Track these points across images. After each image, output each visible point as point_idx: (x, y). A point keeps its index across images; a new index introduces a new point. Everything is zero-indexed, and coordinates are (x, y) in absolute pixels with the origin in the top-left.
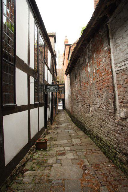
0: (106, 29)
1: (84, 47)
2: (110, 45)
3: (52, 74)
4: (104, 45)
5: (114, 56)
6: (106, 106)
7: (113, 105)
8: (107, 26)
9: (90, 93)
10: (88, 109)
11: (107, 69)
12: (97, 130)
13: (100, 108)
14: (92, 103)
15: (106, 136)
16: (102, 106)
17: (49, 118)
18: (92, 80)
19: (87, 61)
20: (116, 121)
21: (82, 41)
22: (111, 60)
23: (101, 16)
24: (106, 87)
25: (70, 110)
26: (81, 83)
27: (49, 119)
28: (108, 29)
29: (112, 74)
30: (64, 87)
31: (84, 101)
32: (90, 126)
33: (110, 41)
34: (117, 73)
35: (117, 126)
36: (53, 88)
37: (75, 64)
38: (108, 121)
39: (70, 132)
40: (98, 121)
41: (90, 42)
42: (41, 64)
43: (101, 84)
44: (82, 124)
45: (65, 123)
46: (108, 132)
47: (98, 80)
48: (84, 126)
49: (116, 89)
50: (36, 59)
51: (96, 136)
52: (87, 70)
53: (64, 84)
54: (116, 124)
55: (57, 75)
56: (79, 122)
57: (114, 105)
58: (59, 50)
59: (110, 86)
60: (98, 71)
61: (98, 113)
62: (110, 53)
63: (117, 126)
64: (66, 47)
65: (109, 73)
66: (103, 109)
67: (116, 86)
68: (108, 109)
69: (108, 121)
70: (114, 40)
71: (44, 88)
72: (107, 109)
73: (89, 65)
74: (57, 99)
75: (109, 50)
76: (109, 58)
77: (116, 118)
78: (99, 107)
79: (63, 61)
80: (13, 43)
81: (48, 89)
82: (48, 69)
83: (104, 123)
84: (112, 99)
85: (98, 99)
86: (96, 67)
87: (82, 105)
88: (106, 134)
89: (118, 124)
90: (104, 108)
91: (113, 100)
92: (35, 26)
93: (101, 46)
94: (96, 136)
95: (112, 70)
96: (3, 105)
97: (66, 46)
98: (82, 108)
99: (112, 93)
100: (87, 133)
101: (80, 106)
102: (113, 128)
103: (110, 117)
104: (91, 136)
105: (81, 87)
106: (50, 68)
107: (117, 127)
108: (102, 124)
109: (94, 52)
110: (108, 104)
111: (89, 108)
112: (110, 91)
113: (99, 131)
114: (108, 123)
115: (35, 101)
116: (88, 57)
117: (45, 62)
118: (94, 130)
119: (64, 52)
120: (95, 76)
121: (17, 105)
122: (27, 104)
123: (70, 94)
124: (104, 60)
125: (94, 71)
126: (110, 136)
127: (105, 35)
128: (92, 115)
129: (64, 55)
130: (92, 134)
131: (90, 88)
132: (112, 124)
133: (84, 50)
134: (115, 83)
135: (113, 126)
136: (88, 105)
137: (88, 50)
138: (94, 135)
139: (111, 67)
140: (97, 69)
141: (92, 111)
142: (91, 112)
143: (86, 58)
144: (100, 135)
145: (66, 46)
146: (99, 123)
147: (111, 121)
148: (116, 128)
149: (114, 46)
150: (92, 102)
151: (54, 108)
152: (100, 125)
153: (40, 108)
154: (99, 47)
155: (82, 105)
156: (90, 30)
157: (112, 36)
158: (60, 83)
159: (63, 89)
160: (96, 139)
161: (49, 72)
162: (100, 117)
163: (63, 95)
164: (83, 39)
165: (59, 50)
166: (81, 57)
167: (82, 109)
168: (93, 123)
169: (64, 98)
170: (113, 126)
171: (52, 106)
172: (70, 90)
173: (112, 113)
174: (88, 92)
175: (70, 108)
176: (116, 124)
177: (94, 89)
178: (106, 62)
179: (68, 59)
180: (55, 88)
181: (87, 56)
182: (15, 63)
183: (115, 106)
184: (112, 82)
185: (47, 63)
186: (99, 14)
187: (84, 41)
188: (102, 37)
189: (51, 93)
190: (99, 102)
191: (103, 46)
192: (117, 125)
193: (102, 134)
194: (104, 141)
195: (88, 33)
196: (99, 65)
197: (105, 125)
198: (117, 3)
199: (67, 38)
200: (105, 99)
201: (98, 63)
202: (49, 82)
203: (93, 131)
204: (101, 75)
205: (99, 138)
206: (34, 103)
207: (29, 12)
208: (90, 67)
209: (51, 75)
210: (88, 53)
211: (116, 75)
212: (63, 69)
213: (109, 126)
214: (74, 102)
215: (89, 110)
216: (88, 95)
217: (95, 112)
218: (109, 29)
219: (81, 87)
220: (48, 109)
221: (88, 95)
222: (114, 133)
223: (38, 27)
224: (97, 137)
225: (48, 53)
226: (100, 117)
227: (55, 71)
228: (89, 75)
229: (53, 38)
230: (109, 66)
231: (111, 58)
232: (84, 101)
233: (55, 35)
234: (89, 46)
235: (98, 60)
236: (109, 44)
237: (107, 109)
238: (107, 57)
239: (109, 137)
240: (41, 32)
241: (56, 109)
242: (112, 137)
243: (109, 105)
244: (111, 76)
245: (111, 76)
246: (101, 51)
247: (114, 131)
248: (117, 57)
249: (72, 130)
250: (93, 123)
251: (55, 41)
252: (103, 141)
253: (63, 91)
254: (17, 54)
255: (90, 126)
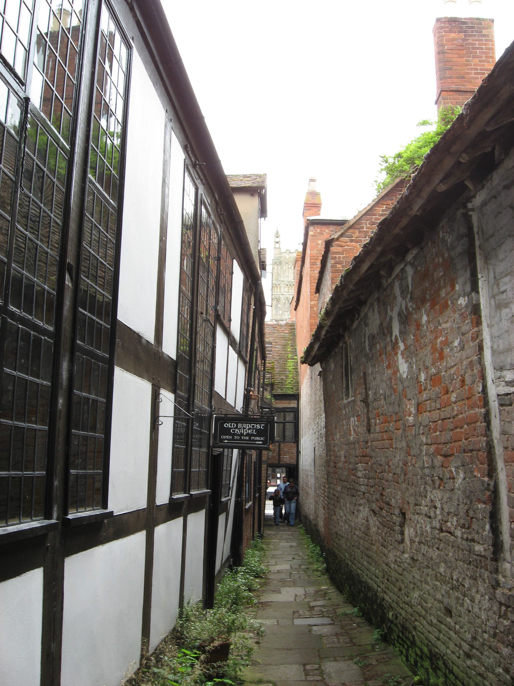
0: (463, 230)
1: (382, 273)
2: (478, 292)
3: (245, 362)
4: (457, 287)
5: (492, 337)
6: (463, 526)
7: (488, 527)
8: (467, 219)
9: (405, 464)
10: (397, 528)
11: (468, 380)
12: (431, 624)
13: (441, 530)
14: (411, 506)
15: (468, 656)
16: (449, 524)
17: (225, 558)
18: (413, 410)
19: (396, 331)
20: (498, 591)
21: (375, 255)
22: (481, 348)
23: (443, 188)
24: (465, 452)
25: (321, 523)
26: (371, 415)
27: (222, 566)
28: (470, 228)
29: (486, 403)
30: (296, 412)
31: (382, 495)
32: (403, 605)
33: (479, 276)
34: (501, 405)
35: (505, 614)
36: (246, 428)
37: (346, 328)
38: (474, 590)
39: (315, 628)
40: (435, 588)
41: (410, 257)
42: (202, 329)
43: (447, 436)
44: (370, 594)
45: (294, 584)
46: (474, 638)
47: (435, 415)
48: (381, 606)
49: (500, 464)
50: (186, 309)
51: (430, 651)
52: (393, 366)
53: (296, 397)
54: (501, 604)
55: (264, 358)
56: (361, 582)
57: (491, 526)
58: (277, 233)
59: (479, 450)
60: (435, 379)
61: (434, 554)
62: (478, 323)
63: (505, 614)
64: (311, 233)
65: (474, 398)
66: (452, 538)
67: (499, 450)
68: (473, 540)
69: (474, 590)
70: (492, 275)
71: (210, 429)
72: (467, 539)
73: (402, 346)
74: (264, 466)
75: (476, 309)
76: (473, 339)
77: (501, 579)
78: (438, 526)
79: (296, 285)
80: (109, 277)
81: (227, 431)
82: (231, 341)
83: (458, 598)
84: (484, 503)
85: (436, 495)
86: (428, 363)
87: (373, 511)
88: (466, 647)
89: (508, 607)
90: (458, 533)
91: (489, 508)
92: (188, 179)
93: (449, 288)
94: (430, 651)
95: (485, 387)
96: (70, 517)
97: (311, 228)
98: (373, 521)
99: (486, 479)
100: (394, 636)
101: (365, 512)
102: (491, 623)
103: (480, 576)
104: (407, 650)
105: (369, 431)
106: (237, 336)
107: (505, 616)
108: (453, 602)
109: (423, 301)
110: (472, 518)
111: (402, 525)
112: (479, 470)
113: (440, 631)
114: (472, 600)
115: (173, 490)
116: (399, 315)
117: (217, 317)
118: (422, 625)
119: (300, 248)
120: (425, 396)
121: (112, 512)
122: (145, 507)
123: (321, 451)
124: (456, 344)
125: (423, 377)
126: (482, 653)
127: (459, 249)
128: (412, 559)
129: (299, 263)
130: (413, 643)
131: (404, 444)
132: (486, 604)
133: (385, 283)
134: (495, 441)
135: (491, 613)
136: (397, 512)
137: (401, 287)
138: (421, 650)
139: (483, 377)
140: (433, 371)
141: (412, 541)
142: (408, 543)
143: (391, 318)
144: (443, 648)
145: (311, 228)
146: (439, 596)
147: (482, 589)
148: (501, 620)
149: (493, 300)
150: (412, 500)
151: (247, 510)
152: (442, 602)
153: (191, 517)
154: (439, 289)
155: (373, 511)
156: (405, 221)
157: (487, 259)
158: (279, 392)
159: (290, 417)
160: (427, 664)
161: (233, 355)
162: (442, 570)
163: (288, 448)
164: (379, 249)
165: (277, 233)
166: (372, 305)
167: (374, 530)
168: (416, 594)
169: (294, 461)
170: (491, 613)
171: (239, 505)
172: (323, 431)
173: (484, 556)
174: (398, 458)
175: (321, 512)
176: (501, 604)
177: (421, 451)
178: (464, 354)
179: (318, 290)
180: (260, 433)
181: (396, 310)
182: (112, 353)
183: (496, 530)
184: (486, 435)
185: (225, 322)
186: (437, 181)
187: (383, 253)
188: (453, 254)
189: (235, 451)
190: (439, 505)
191: (453, 287)
192: (503, 608)
193: (452, 645)
194: (461, 675)
195: (397, 230)
196: (442, 357)
197: (462, 605)
198: (497, 154)
199: (317, 187)
200: (461, 500)
201: (434, 349)
202: (230, 400)
203: (415, 628)
204: (445, 397)
205: (440, 663)
206: (171, 499)
207: (168, 134)
208: (408, 354)
209: (241, 365)
210: (399, 299)
211: (500, 411)
212: (292, 327)
213: (476, 610)
214: (339, 489)
215: (402, 533)
216: (398, 471)
217: (424, 549)
218: (476, 230)
219: (369, 431)
220: (222, 518)
221: (398, 471)
222: (494, 643)
223: (198, 182)
224: (431, 659)
225: (232, 273)
226: (442, 570)
227: (256, 345)
228: (400, 388)
229: (255, 202)
230: (475, 371)
231: (482, 341)
232: (382, 495)
233: (263, 188)
234: (403, 270)
235: (436, 338)
236: (475, 288)
237: (467, 539)
238: (469, 336)
239: (479, 660)
240: (207, 200)
241: (256, 515)
242: (489, 658)
243: (475, 526)
244: (483, 410)
245: (483, 410)
246: (446, 306)
247: (495, 635)
248: (500, 341)
249: (326, 621)
250: (416, 594)
251: (263, 212)
252: (457, 678)
253: (289, 432)
254: (121, 317)
255: (403, 605)
